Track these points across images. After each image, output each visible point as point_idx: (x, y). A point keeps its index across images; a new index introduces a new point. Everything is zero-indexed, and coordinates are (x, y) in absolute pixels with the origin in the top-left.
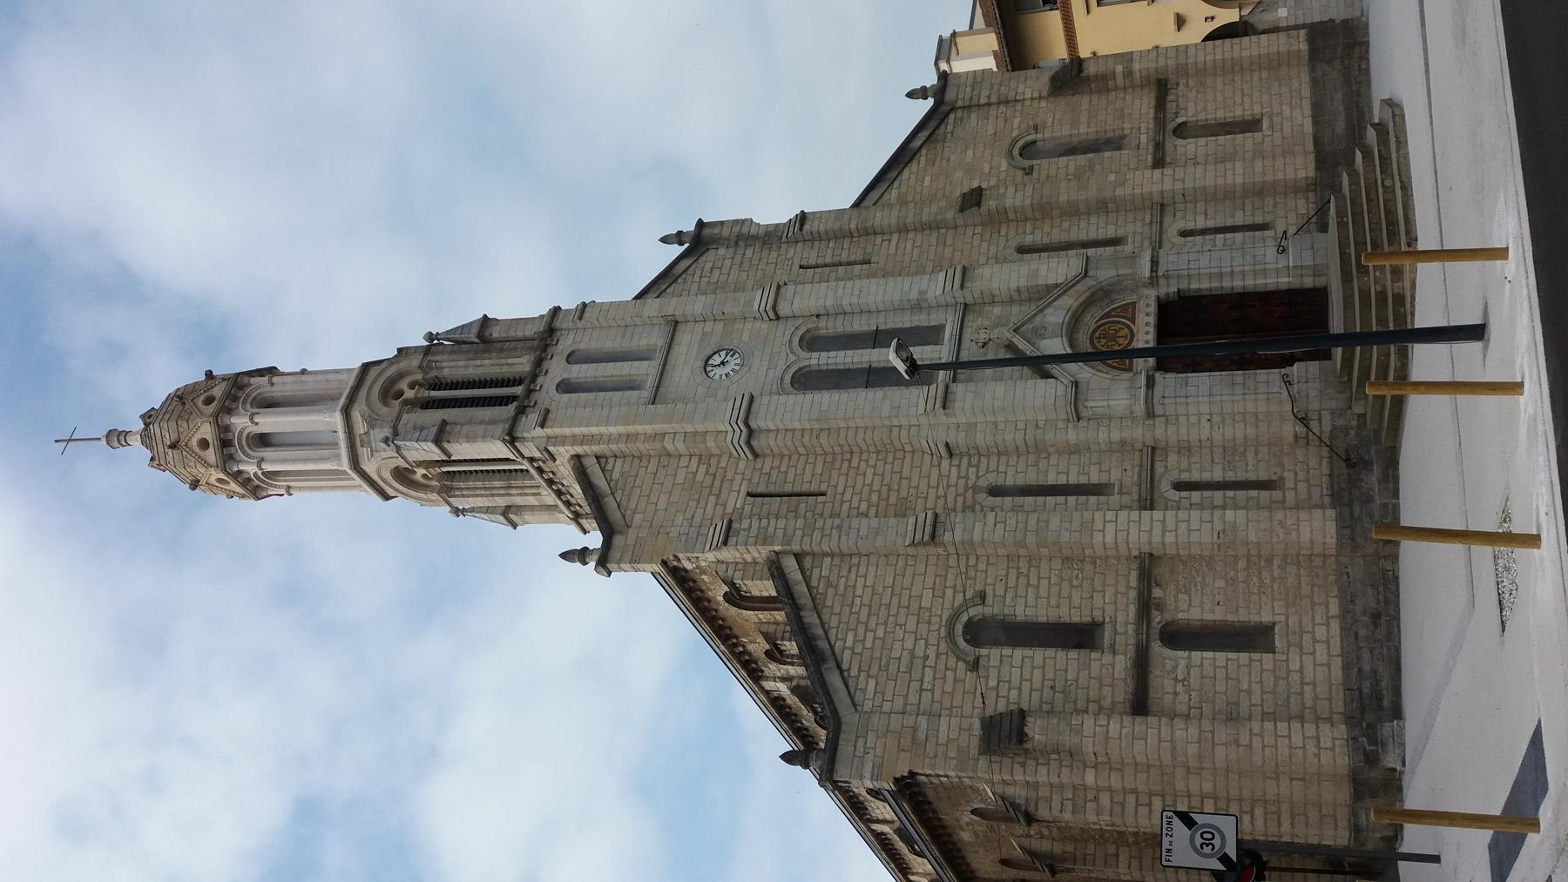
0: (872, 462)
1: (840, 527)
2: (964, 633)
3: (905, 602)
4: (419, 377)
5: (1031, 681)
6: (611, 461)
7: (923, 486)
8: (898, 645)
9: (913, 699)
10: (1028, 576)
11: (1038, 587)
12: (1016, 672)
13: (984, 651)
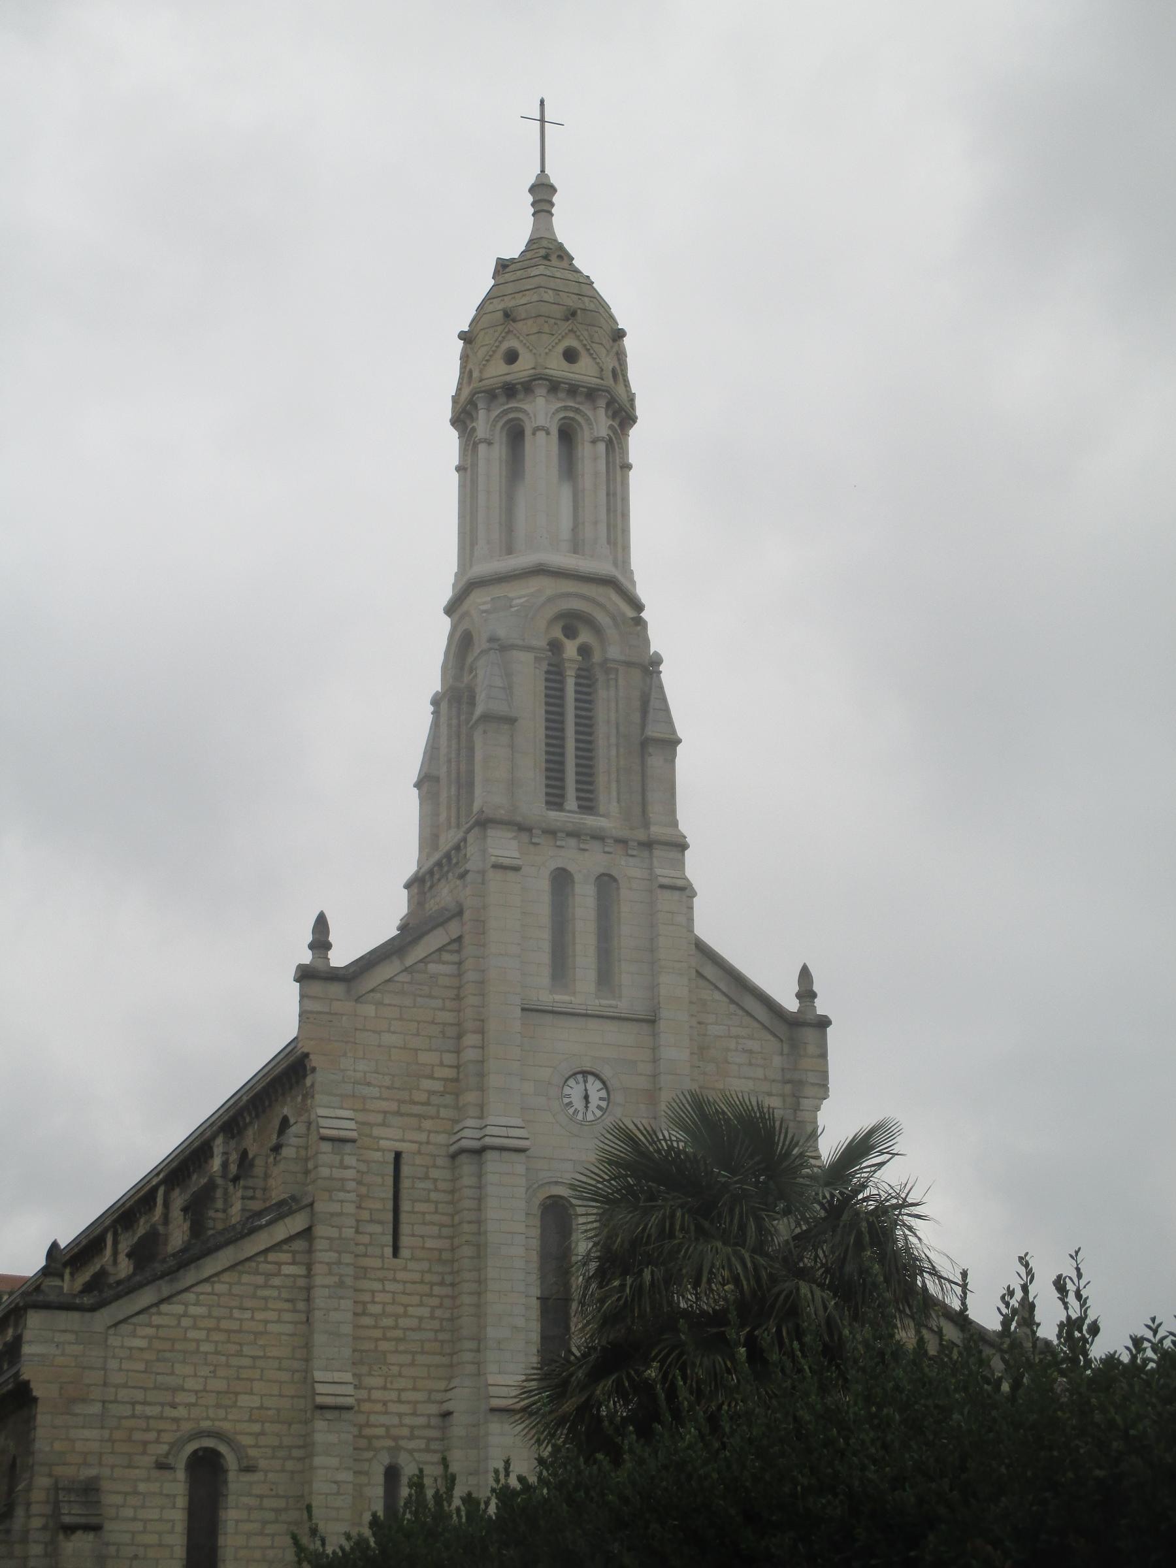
0: (438, 1313)
1: (341, 1284)
2: (206, 1449)
3: (245, 1374)
4: (597, 657)
5: (144, 1532)
6: (455, 958)
7: (401, 1383)
8: (188, 1370)
9: (123, 1394)
10: (276, 1521)
11: (262, 1534)
12: (154, 1514)
13: (181, 1475)
